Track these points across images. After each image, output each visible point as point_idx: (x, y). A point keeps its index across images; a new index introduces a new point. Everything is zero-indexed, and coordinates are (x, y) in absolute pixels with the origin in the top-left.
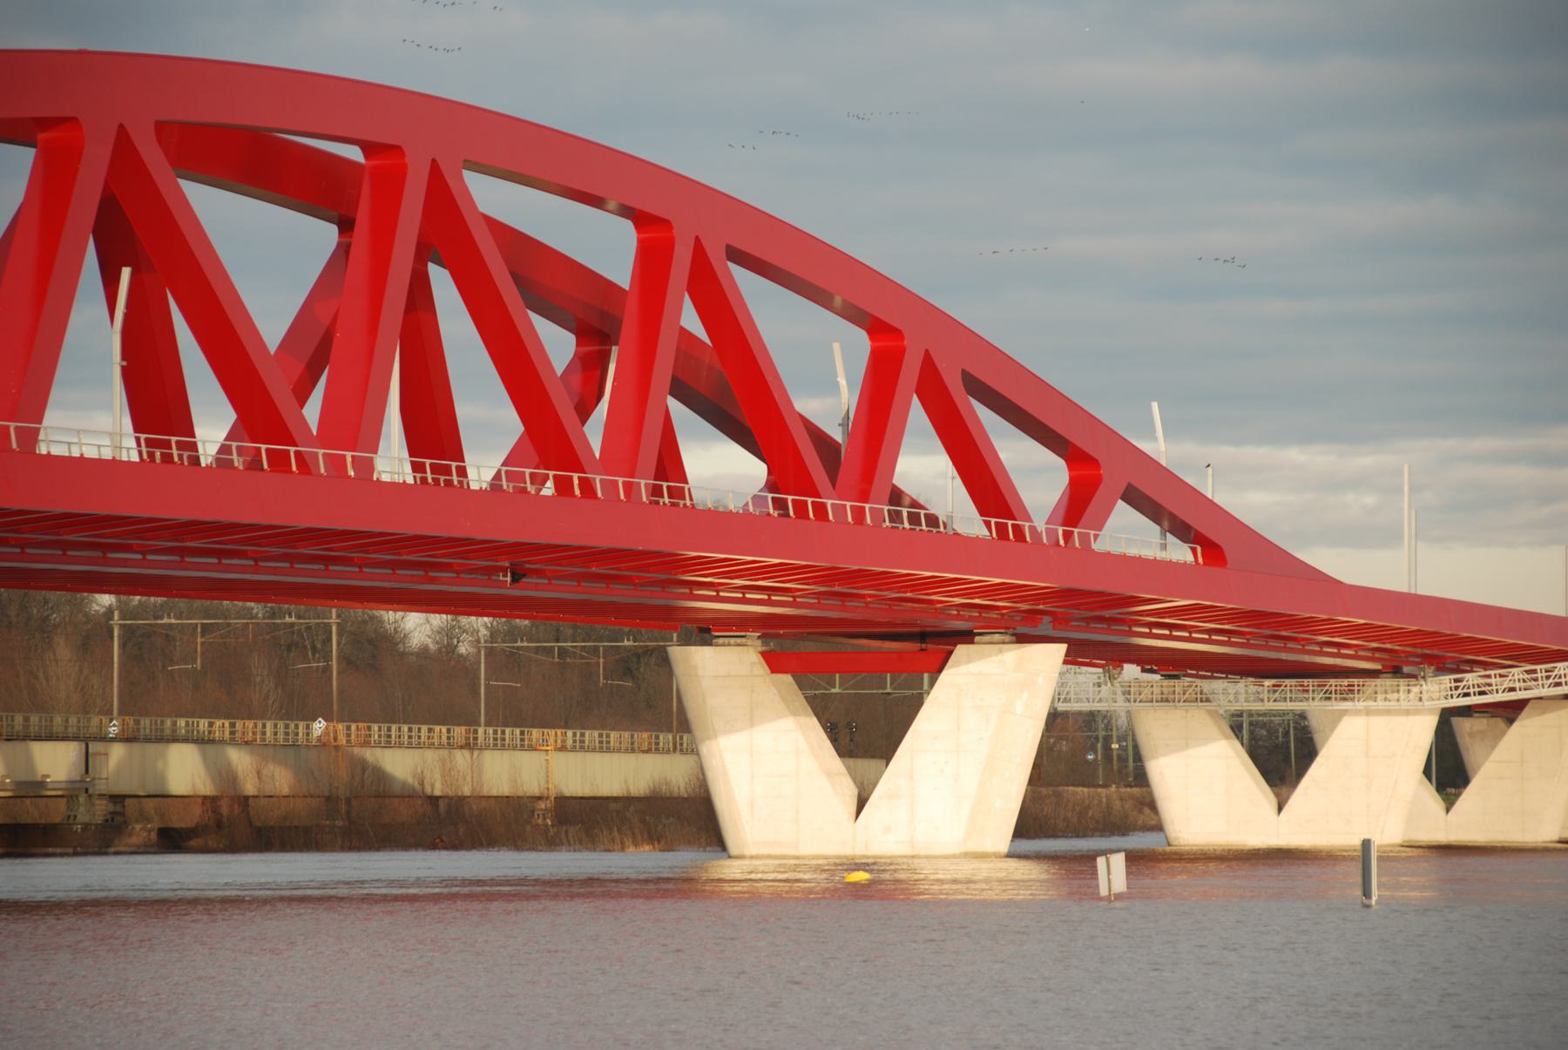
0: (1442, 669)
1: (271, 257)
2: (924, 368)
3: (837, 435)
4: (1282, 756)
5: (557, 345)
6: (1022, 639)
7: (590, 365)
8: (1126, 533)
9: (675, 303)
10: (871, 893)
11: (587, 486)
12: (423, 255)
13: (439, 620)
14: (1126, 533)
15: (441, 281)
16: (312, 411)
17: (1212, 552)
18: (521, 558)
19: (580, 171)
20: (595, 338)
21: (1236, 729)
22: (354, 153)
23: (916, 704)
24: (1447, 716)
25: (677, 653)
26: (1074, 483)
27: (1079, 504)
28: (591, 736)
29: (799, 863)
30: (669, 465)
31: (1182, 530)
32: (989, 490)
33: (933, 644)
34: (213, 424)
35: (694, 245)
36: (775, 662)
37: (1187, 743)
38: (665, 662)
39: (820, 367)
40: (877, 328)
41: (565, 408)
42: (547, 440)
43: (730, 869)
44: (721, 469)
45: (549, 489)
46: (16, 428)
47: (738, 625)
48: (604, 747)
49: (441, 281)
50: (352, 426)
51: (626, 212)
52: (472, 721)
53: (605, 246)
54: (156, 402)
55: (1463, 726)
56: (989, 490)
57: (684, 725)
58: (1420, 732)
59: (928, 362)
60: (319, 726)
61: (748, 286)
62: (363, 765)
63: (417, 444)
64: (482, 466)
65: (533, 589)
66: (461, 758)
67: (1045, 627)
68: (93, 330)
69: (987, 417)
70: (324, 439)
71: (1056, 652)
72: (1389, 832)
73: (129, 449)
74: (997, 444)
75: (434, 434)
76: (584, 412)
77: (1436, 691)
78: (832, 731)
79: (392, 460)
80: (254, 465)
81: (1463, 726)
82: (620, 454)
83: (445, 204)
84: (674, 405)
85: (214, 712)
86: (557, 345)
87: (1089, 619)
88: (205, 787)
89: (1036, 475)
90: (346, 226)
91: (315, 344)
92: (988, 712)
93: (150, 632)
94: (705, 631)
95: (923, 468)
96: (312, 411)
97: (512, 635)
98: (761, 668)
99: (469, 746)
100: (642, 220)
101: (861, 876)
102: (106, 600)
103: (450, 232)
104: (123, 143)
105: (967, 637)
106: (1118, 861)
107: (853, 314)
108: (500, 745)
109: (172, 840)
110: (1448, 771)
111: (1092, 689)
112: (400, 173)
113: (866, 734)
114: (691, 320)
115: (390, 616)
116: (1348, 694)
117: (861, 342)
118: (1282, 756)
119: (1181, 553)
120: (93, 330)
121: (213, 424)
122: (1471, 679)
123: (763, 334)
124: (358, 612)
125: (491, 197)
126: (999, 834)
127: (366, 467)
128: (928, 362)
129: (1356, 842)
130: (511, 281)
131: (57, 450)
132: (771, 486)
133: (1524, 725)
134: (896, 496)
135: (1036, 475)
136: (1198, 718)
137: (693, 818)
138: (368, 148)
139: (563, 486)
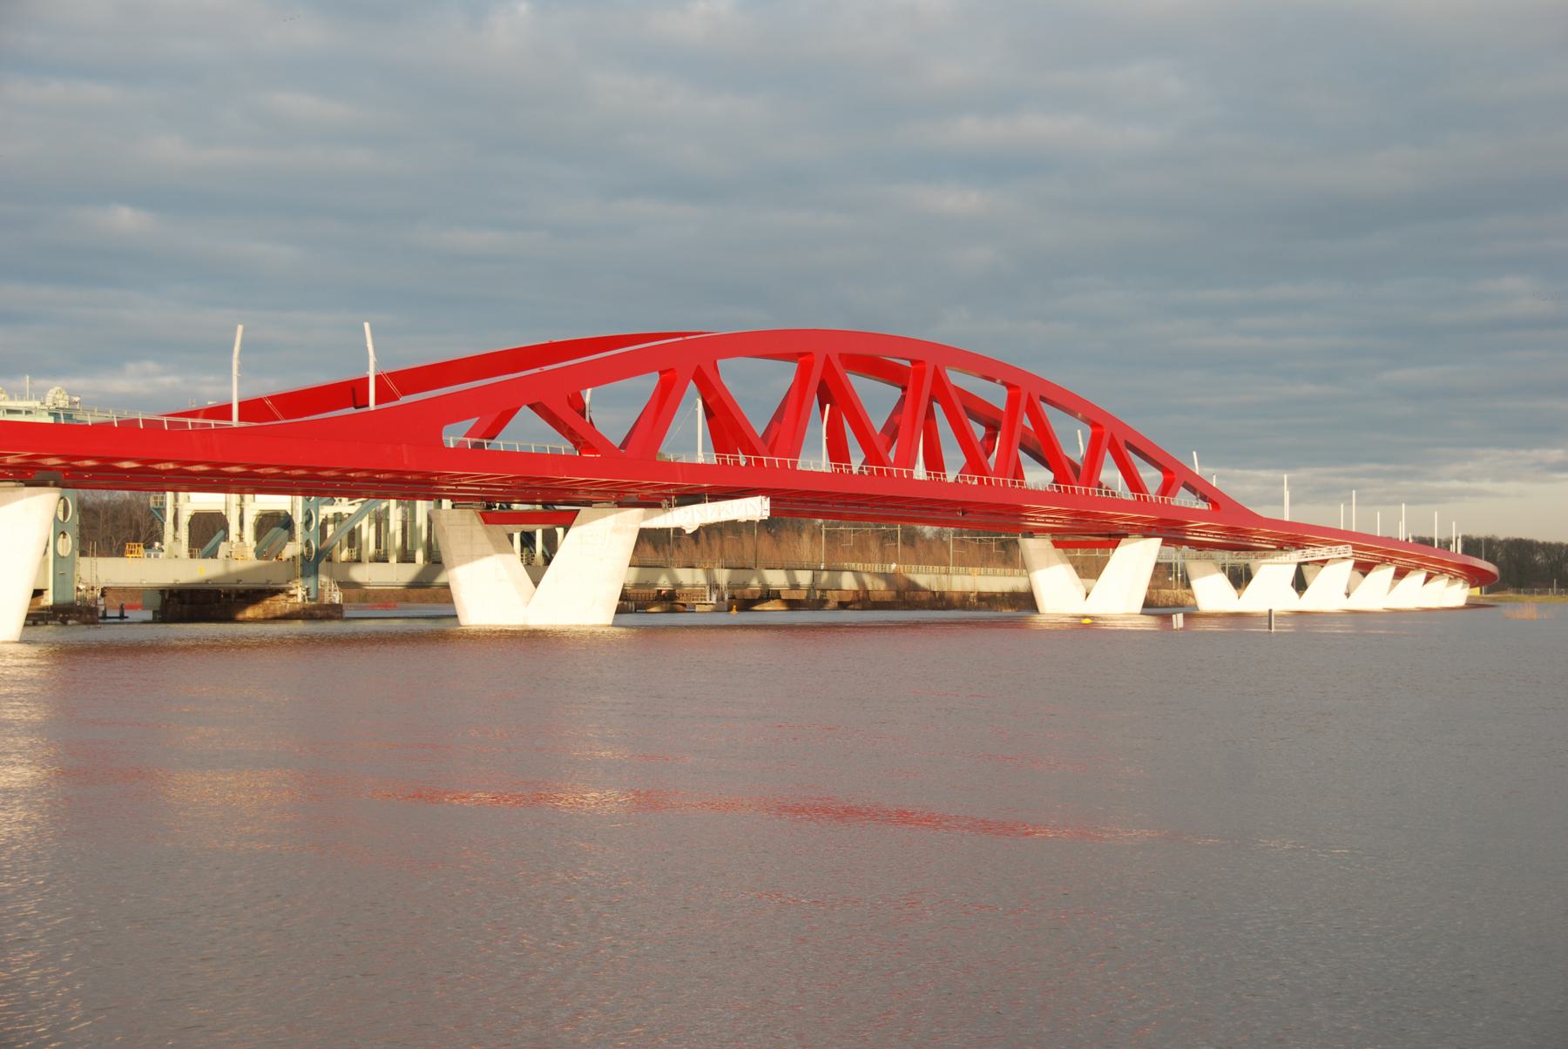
0: (1298, 548)
1: (877, 399)
2: (1112, 439)
3: (1079, 462)
4: (1240, 578)
5: (979, 431)
6: (1146, 536)
7: (991, 437)
8: (1184, 499)
9: (1020, 416)
10: (1086, 630)
11: (989, 481)
12: (931, 399)
13: (936, 528)
14: (1184, 499)
15: (937, 407)
16: (892, 455)
17: (1215, 505)
18: (966, 507)
19: (988, 369)
20: (992, 429)
21: (1223, 569)
22: (908, 364)
23: (1108, 559)
24: (1300, 565)
25: (1021, 540)
26: (1165, 481)
27: (1166, 489)
28: (990, 570)
29: (1064, 616)
30: (1018, 474)
31: (1204, 498)
32: (1134, 483)
33: (1113, 538)
34: (857, 460)
35: (1030, 397)
36: (1056, 544)
37: (1205, 574)
38: (1016, 542)
39: (1075, 441)
40: (1094, 425)
41: (981, 452)
42: (975, 465)
43: (1037, 618)
44: (1038, 477)
45: (975, 482)
46: (230, 419)
47: (1044, 531)
48: (995, 574)
49: (937, 407)
50: (908, 461)
51: (1004, 383)
52: (947, 565)
53: (995, 395)
54: (838, 452)
55: (1305, 568)
56: (1134, 483)
57: (1024, 567)
58: (1291, 571)
59: (1112, 439)
60: (894, 566)
61: (1049, 411)
62: (909, 581)
63: (928, 467)
64: (951, 476)
65: (968, 518)
66: (944, 577)
67: (1154, 532)
68: (817, 429)
69: (1135, 459)
70: (996, 473)
71: (1160, 540)
72: (1278, 608)
73: (713, 459)
74: (1139, 469)
75: (934, 462)
76: (988, 454)
77: (1296, 556)
78: (1076, 568)
79: (920, 472)
80: (871, 473)
81: (1305, 568)
82: (1001, 470)
83: (939, 381)
84: (1022, 455)
85: (857, 560)
86: (979, 431)
87: (1171, 529)
88: (855, 587)
89: (1151, 477)
90: (904, 389)
91: (892, 430)
92: (1135, 560)
93: (835, 533)
94: (1031, 533)
95: (1110, 475)
96: (892, 455)
97: (961, 534)
98: (1051, 546)
99: (947, 573)
100: (1009, 386)
101: (1087, 621)
102: (820, 521)
103: (941, 391)
104: (828, 360)
105: (1126, 536)
106: (1180, 616)
107: (1086, 420)
108: (958, 573)
109: (843, 605)
110: (1300, 584)
111: (1174, 555)
112: (811, 364)
113: (1090, 571)
114: (1027, 422)
115: (918, 527)
116: (1264, 557)
117: (1089, 430)
118: (1240, 578)
119: (1203, 506)
120: (817, 429)
121: (857, 460)
122: (1309, 551)
123: (1142, 433)
124: (907, 525)
125: (958, 379)
126: (1138, 607)
127: (794, 464)
128: (1112, 439)
129: (1265, 610)
130: (964, 408)
131: (671, 457)
132: (1055, 481)
133: (1327, 568)
134: (1100, 485)
135: (1151, 477)
136: (1209, 565)
137: (1026, 601)
138: (913, 362)
139: (981, 481)
